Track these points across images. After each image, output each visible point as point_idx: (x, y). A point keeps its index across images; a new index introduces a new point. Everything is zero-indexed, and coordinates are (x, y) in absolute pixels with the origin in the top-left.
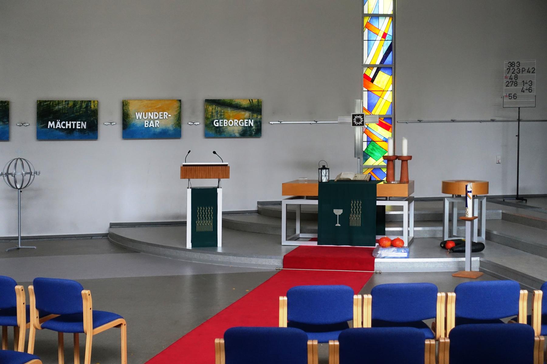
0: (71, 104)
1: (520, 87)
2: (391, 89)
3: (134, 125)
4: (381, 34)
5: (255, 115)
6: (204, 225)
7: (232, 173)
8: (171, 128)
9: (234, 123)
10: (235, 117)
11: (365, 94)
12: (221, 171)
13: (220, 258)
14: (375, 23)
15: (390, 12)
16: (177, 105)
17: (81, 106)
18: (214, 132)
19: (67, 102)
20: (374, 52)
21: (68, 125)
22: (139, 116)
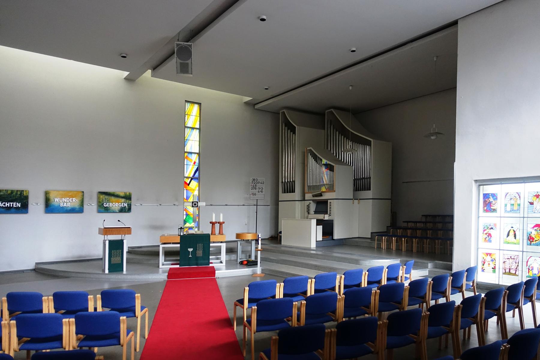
0: (9, 192)
1: (257, 190)
2: (197, 189)
3: (53, 205)
4: (193, 162)
5: (128, 201)
6: (116, 260)
7: (133, 231)
8: (78, 207)
9: (116, 205)
10: (116, 202)
11: (185, 191)
12: (127, 230)
13: (125, 277)
14: (190, 155)
15: (198, 152)
16: (81, 194)
17: (16, 194)
18: (103, 209)
19: (7, 191)
20: (190, 171)
21: (7, 205)
22: (57, 200)
